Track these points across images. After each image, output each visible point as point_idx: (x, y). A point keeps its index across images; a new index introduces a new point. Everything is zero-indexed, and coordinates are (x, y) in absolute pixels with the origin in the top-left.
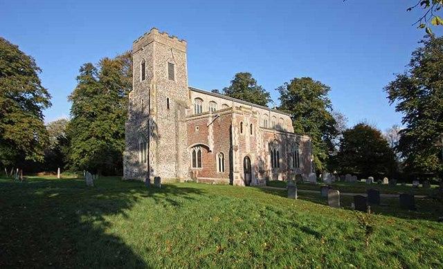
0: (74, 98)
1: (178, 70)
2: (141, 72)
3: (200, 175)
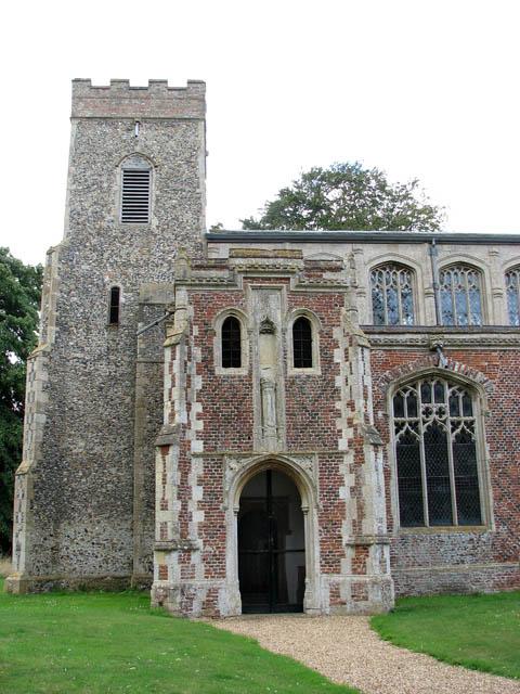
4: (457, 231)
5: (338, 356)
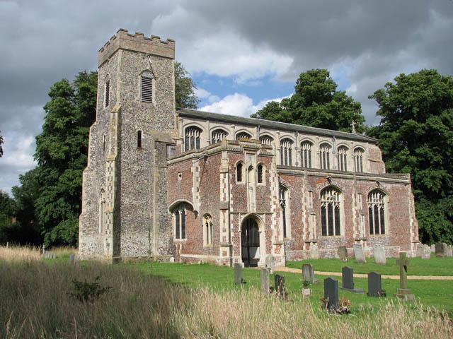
0: (39, 140)
1: (158, 87)
2: (105, 94)
4: (232, 114)
5: (271, 180)
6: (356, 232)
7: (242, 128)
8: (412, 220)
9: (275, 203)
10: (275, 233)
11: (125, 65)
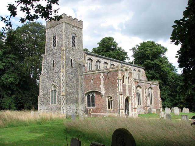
1: (78, 41)
2: (52, 41)
3: (93, 112)
6: (145, 104)
7: (98, 59)
8: (159, 99)
9: (133, 92)
10: (134, 104)
11: (66, 30)
